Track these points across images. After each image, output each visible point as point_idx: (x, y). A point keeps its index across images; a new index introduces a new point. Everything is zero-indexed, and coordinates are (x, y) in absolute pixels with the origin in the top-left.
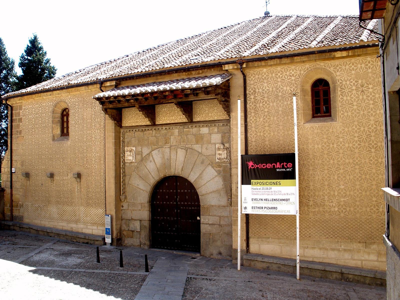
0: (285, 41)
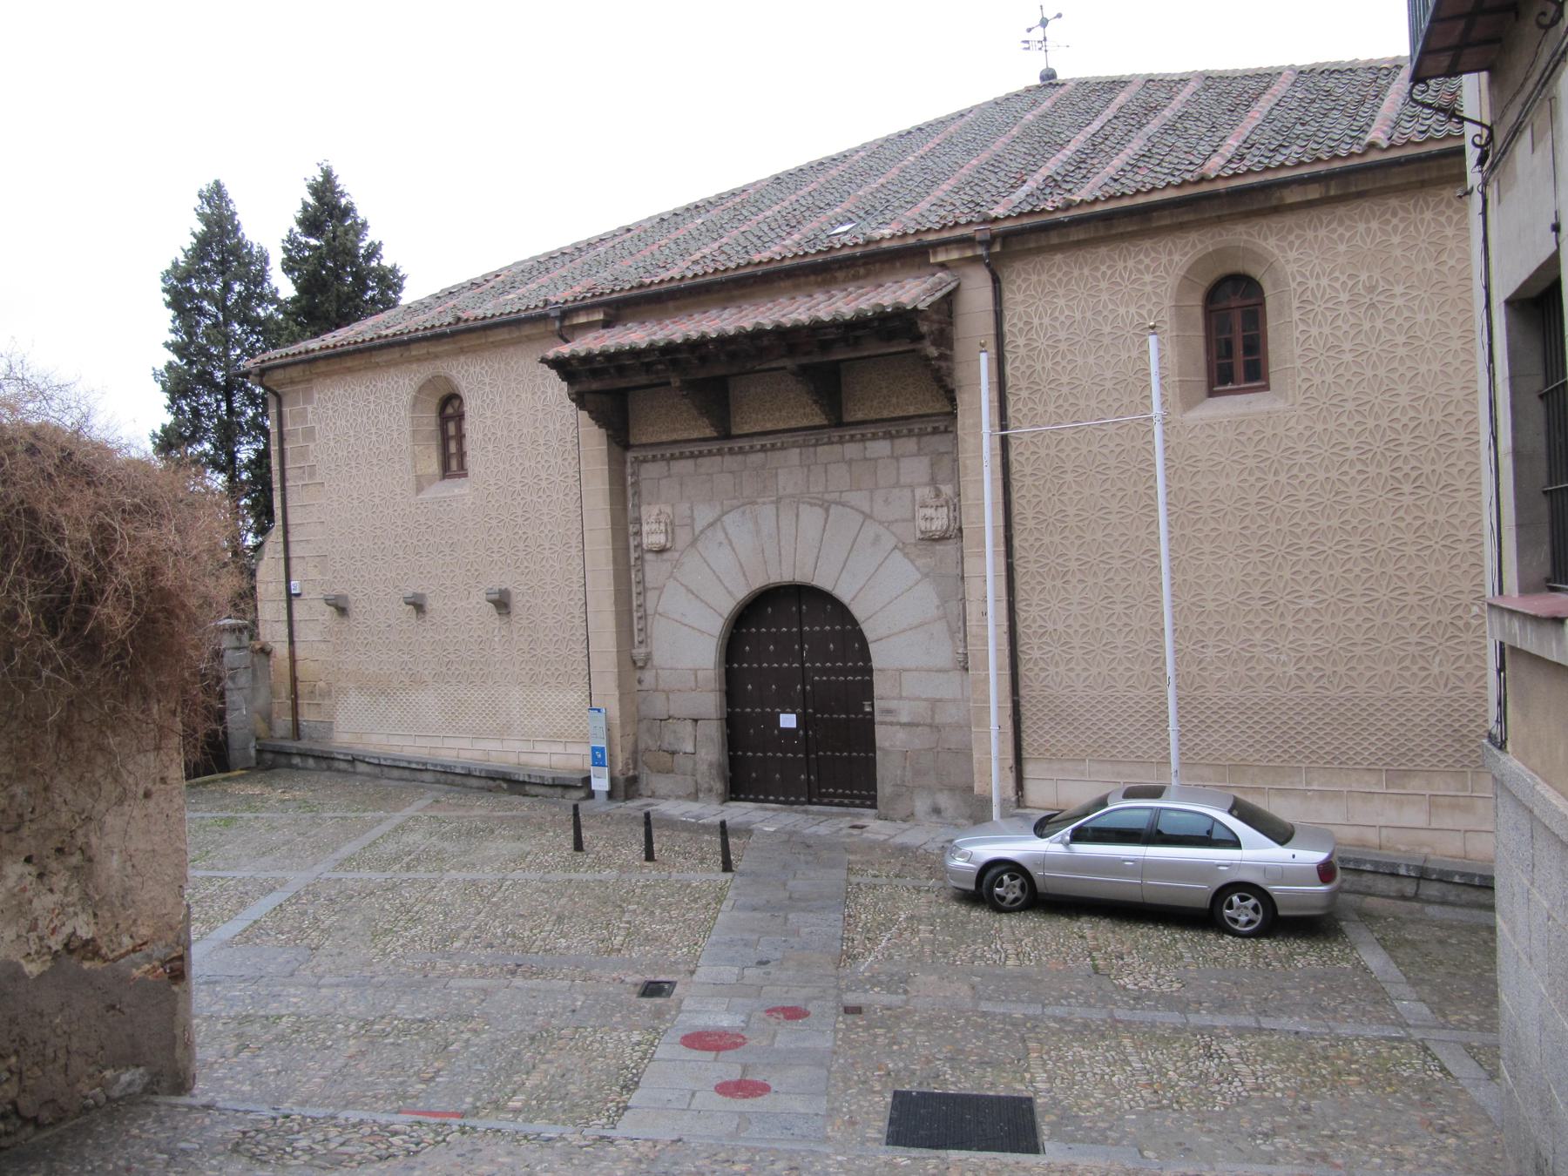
0: (1117, 162)
